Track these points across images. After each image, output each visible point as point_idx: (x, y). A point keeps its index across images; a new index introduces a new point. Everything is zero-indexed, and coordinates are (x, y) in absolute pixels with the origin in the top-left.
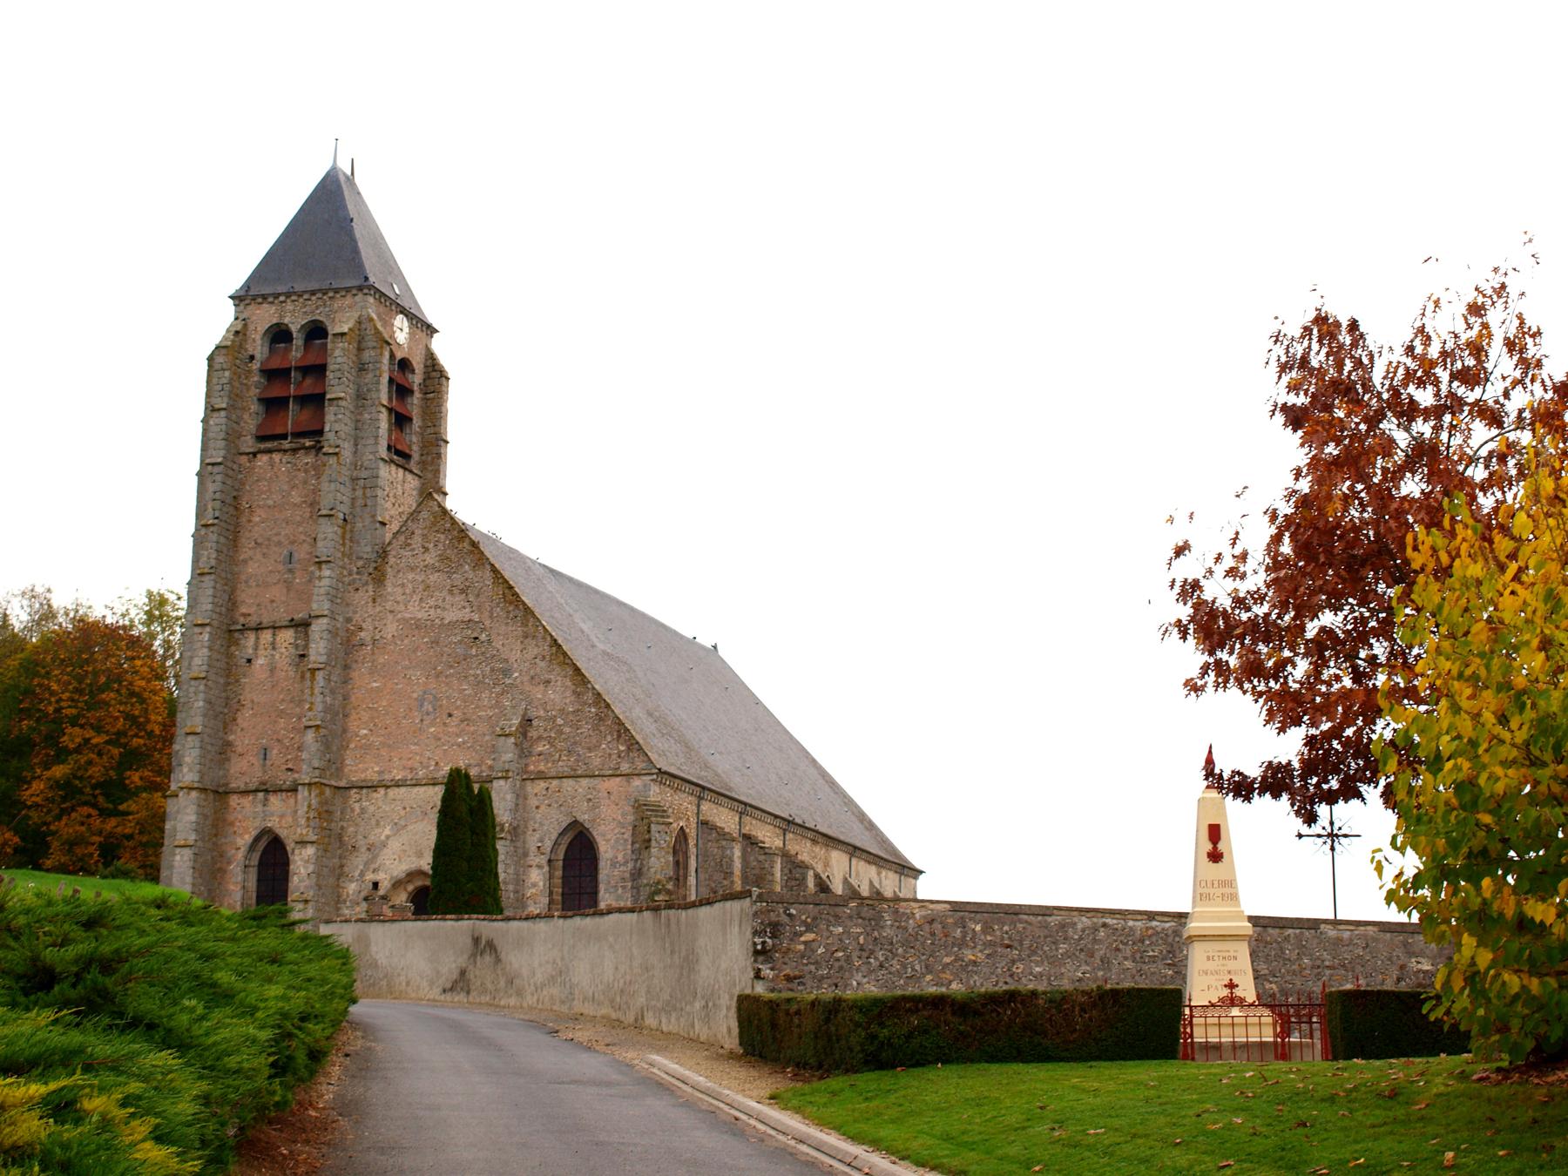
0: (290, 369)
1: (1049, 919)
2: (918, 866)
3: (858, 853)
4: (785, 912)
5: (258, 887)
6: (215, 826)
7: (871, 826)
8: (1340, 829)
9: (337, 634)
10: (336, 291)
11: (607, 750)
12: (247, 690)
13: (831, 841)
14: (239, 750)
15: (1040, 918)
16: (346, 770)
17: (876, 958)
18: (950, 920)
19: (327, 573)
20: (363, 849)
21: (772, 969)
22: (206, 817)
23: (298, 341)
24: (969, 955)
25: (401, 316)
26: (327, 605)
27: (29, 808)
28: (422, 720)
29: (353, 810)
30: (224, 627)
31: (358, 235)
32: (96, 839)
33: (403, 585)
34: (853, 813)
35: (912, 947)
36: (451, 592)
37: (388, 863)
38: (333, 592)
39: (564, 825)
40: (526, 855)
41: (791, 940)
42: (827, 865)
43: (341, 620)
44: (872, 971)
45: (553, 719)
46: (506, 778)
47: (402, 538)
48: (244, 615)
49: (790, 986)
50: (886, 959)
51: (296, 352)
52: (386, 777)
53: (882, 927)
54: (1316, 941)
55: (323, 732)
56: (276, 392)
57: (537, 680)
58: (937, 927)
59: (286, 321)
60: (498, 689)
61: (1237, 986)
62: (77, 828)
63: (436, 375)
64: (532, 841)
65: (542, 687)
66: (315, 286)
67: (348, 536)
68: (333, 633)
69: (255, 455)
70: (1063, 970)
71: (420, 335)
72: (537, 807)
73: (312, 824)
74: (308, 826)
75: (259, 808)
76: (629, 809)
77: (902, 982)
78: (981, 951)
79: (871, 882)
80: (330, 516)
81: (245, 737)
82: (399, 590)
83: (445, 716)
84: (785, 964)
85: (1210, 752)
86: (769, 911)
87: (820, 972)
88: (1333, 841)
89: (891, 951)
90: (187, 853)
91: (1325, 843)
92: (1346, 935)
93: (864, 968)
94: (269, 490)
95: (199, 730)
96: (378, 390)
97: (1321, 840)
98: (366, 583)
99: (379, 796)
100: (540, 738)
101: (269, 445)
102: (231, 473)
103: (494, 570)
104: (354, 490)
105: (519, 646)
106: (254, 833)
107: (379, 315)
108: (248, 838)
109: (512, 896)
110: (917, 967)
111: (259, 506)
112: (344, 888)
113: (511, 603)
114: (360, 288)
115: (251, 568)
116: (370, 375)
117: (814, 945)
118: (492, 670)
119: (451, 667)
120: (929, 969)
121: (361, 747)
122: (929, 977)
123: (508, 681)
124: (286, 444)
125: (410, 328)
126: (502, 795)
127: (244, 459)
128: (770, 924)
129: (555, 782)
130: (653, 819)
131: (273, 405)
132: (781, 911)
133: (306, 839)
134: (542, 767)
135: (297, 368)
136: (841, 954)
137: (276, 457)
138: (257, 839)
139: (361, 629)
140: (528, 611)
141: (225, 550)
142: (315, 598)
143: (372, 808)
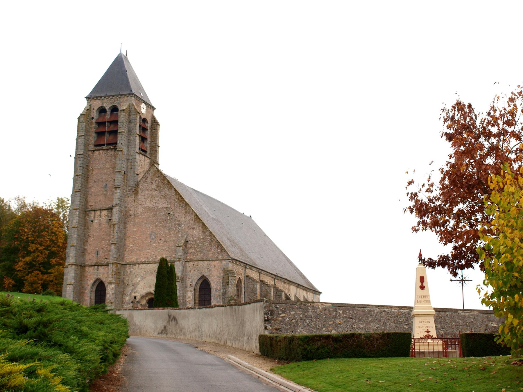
1: (365, 309)
2: (320, 291)
3: (300, 286)
4: (275, 306)
6: (80, 278)
7: (304, 277)
9: (122, 212)
10: (121, 95)
13: (290, 282)
14: (89, 251)
15: (362, 309)
16: (125, 258)
17: (306, 322)
18: (331, 309)
19: (118, 191)
20: (131, 285)
21: (271, 326)
23: (108, 112)
24: (338, 321)
25: (143, 104)
28: (151, 241)
29: (127, 272)
30: (84, 210)
33: (144, 195)
34: (298, 273)
35: (319, 319)
36: (160, 197)
37: (139, 290)
39: (199, 277)
40: (186, 287)
41: (277, 316)
42: (289, 290)
43: (123, 207)
45: (196, 241)
47: (144, 179)
48: (91, 206)
49: (276, 331)
50: (310, 323)
51: (108, 116)
52: (139, 261)
55: (117, 245)
56: (101, 130)
58: (327, 312)
59: (104, 105)
60: (177, 231)
61: (430, 332)
63: (155, 124)
64: (188, 282)
65: (191, 230)
67: (126, 179)
68: (121, 212)
69: (94, 151)
70: (370, 326)
72: (190, 271)
73: (114, 277)
74: (112, 277)
75: (96, 271)
77: (315, 330)
78: (342, 320)
81: (91, 247)
82: (143, 197)
83: (159, 240)
84: (275, 324)
85: (420, 252)
87: (287, 327)
88: (463, 282)
89: (311, 320)
90: (71, 286)
92: (467, 314)
93: (302, 326)
95: (75, 245)
96: (136, 129)
98: (132, 195)
99: (136, 267)
100: (191, 247)
101: (99, 148)
103: (175, 190)
104: (128, 163)
106: (94, 280)
107: (136, 104)
108: (92, 282)
109: (181, 301)
110: (320, 325)
111: (95, 169)
114: (129, 94)
115: (93, 190)
117: (285, 318)
118: (175, 224)
121: (130, 251)
122: (324, 329)
123: (180, 228)
124: (104, 147)
125: (146, 108)
126: (178, 267)
127: (90, 153)
128: (270, 311)
129: (196, 262)
130: (230, 275)
131: (100, 134)
132: (274, 306)
133: (111, 282)
134: (192, 257)
135: (108, 122)
137: (101, 152)
138: (95, 282)
139: (130, 210)
140: (187, 204)
143: (134, 271)
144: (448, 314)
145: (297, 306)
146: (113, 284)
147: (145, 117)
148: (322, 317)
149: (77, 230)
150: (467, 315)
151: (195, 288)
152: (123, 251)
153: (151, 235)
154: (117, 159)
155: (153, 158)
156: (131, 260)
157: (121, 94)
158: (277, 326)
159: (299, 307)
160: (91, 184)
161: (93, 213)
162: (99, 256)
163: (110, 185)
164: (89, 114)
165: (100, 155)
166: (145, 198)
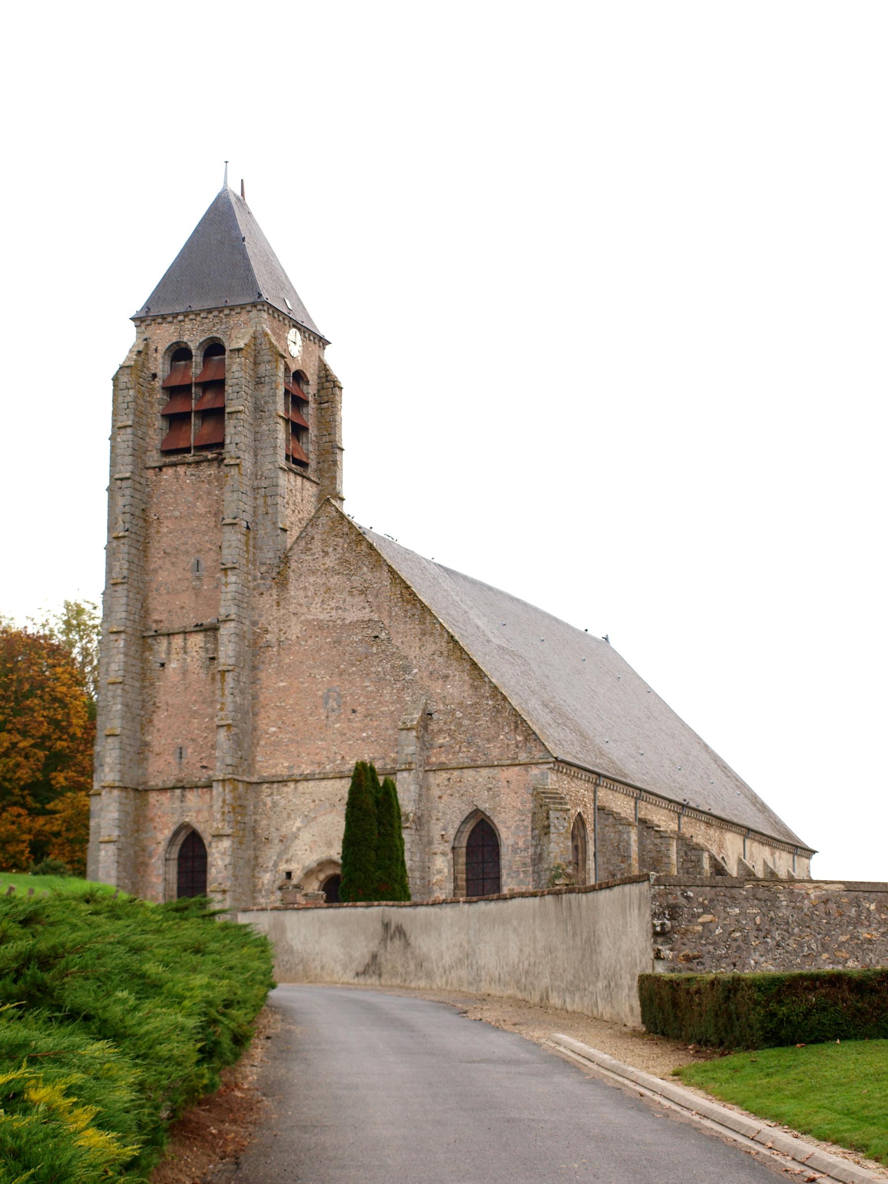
2: (812, 846)
3: (751, 835)
7: (763, 809)
9: (244, 637)
10: (231, 309)
12: (162, 692)
13: (725, 824)
14: (157, 750)
16: (257, 766)
17: (773, 938)
18: (845, 900)
19: (232, 578)
20: (276, 841)
21: (671, 950)
22: (127, 814)
23: (197, 358)
24: (864, 934)
25: (294, 330)
28: (327, 717)
29: (265, 804)
30: (138, 634)
31: (250, 253)
32: (26, 837)
33: (305, 588)
35: (808, 927)
36: (351, 593)
37: (299, 853)
38: (239, 597)
39: (466, 813)
40: (430, 843)
41: (689, 921)
42: (721, 846)
43: (248, 623)
46: (409, 770)
47: (303, 543)
49: (689, 965)
50: (783, 938)
51: (196, 369)
52: (296, 771)
55: (234, 730)
56: (179, 407)
57: (436, 675)
58: (832, 906)
59: (185, 339)
64: (436, 830)
65: (440, 682)
66: (212, 305)
67: (251, 543)
68: (241, 636)
69: (160, 468)
72: (440, 797)
73: (227, 818)
74: (224, 820)
75: (177, 804)
77: (799, 960)
78: (876, 930)
79: (765, 863)
82: (301, 593)
83: (349, 712)
84: (684, 944)
86: (667, 894)
90: (112, 848)
93: (761, 948)
94: (175, 502)
95: (118, 732)
96: (275, 402)
98: (270, 588)
99: (289, 790)
100: (440, 731)
101: (173, 459)
102: (138, 486)
103: (391, 571)
104: (256, 499)
105: (417, 644)
106: (173, 828)
107: (273, 330)
108: (168, 833)
109: (418, 882)
110: (814, 946)
112: (259, 878)
113: (408, 602)
114: (254, 305)
115: (161, 577)
116: (267, 388)
117: (712, 926)
118: (393, 667)
119: (353, 665)
120: (825, 948)
121: (271, 744)
122: (825, 956)
123: (408, 677)
124: (189, 458)
125: (303, 341)
126: (406, 786)
127: (150, 473)
128: (668, 907)
129: (456, 773)
130: (552, 806)
132: (679, 893)
133: (222, 832)
134: (443, 759)
135: (197, 384)
136: (738, 934)
137: (181, 470)
138: (176, 834)
139: (267, 632)
140: (425, 609)
141: (136, 560)
142: (222, 603)
143: (283, 802)
146: (225, 839)
147: (301, 368)
149: (123, 689)
151: (456, 845)
152: (250, 747)
153: (326, 699)
156: (273, 771)
158: (690, 949)
160: (155, 562)
161: (164, 641)
162: (184, 761)
163: (208, 561)
164: (143, 365)
165: (177, 477)
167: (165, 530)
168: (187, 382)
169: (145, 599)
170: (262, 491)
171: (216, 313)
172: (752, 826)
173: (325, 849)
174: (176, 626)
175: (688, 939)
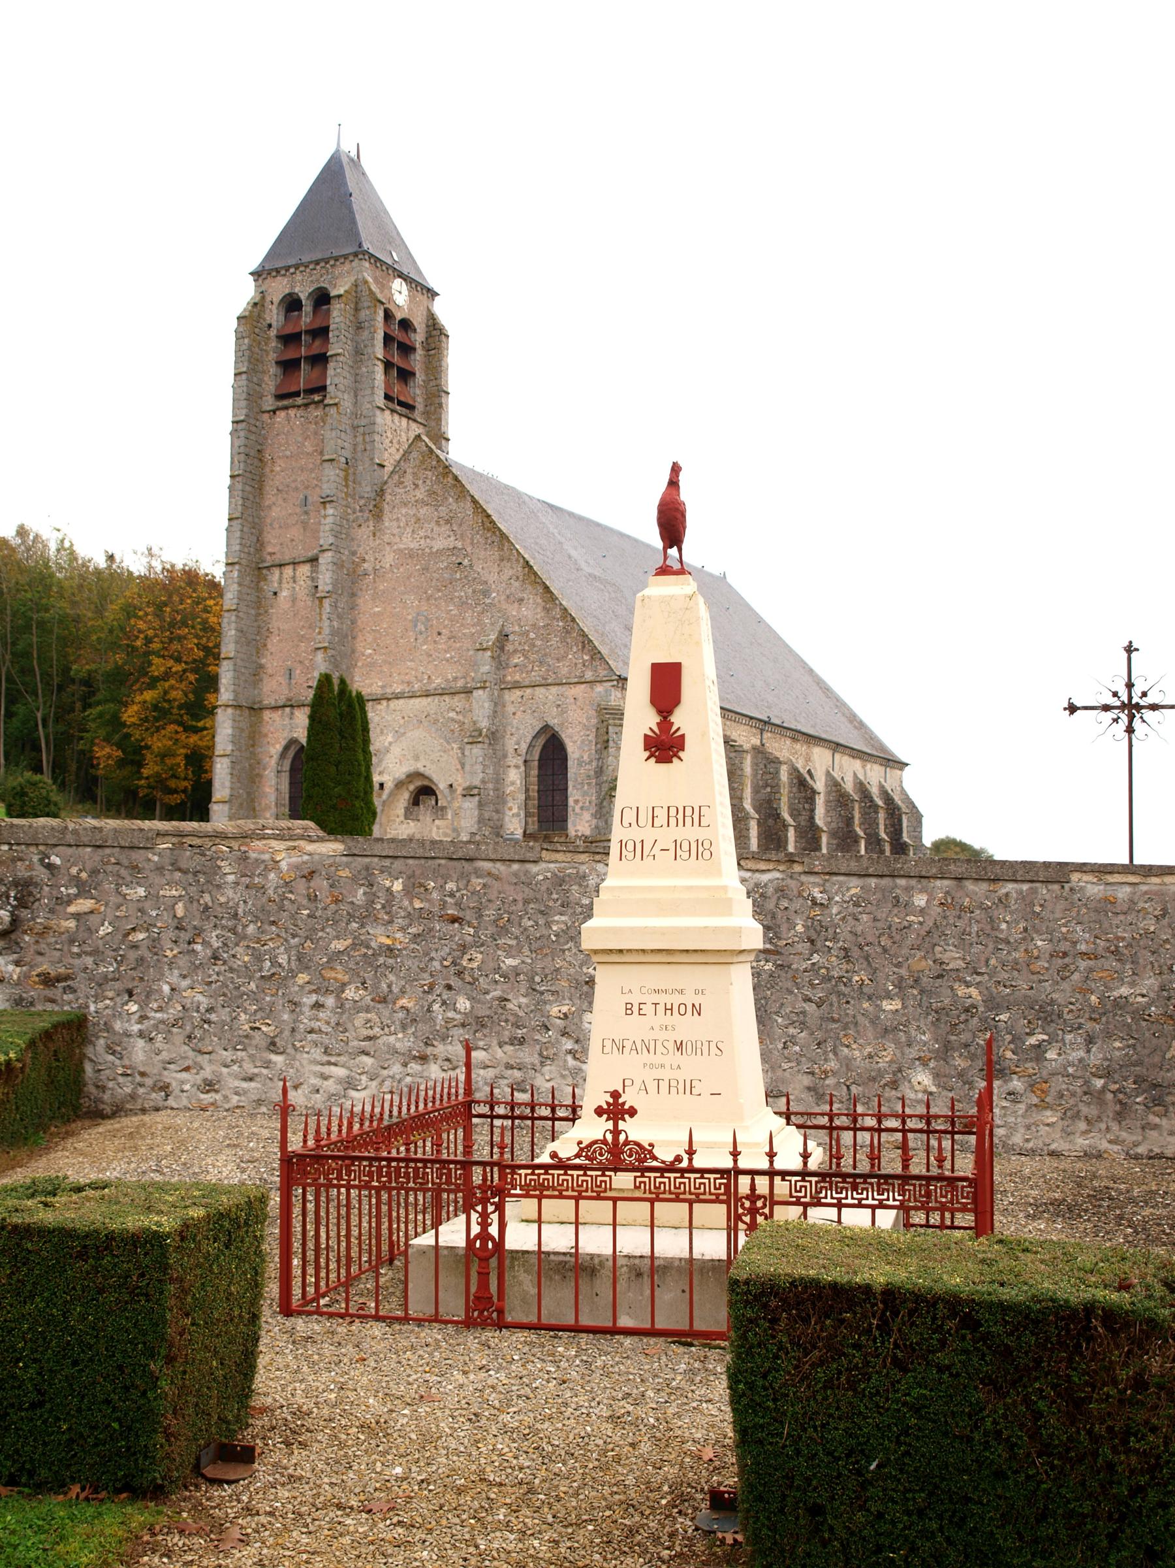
0: (300, 333)
1: (534, 868)
2: (904, 760)
3: (841, 749)
4: (41, 860)
5: (291, 788)
6: (250, 738)
7: (860, 726)
8: (1144, 694)
9: (343, 566)
10: (336, 259)
11: (571, 661)
12: (274, 618)
13: (813, 739)
14: (270, 671)
15: (516, 866)
17: (206, 944)
18: (345, 873)
19: (330, 511)
21: (17, 963)
22: (242, 730)
23: (308, 307)
24: (379, 936)
25: (399, 280)
26: (331, 540)
27: (129, 726)
30: (254, 565)
31: (355, 207)
32: (183, 751)
33: (398, 519)
34: (843, 714)
35: (273, 923)
36: (438, 523)
39: (537, 729)
40: (505, 756)
41: (52, 911)
42: (808, 759)
43: (346, 553)
44: (197, 967)
45: (527, 633)
46: (484, 688)
47: (396, 477)
48: (271, 554)
49: (49, 993)
50: (225, 944)
51: (306, 318)
52: (389, 690)
53: (219, 887)
54: (1062, 905)
55: (331, 652)
56: (291, 354)
57: (512, 599)
58: (321, 884)
59: (296, 290)
60: (479, 609)
61: (632, 1112)
62: (165, 742)
63: (436, 332)
64: (510, 744)
65: (516, 604)
66: (320, 256)
67: (351, 478)
68: (338, 565)
69: (274, 412)
70: (559, 963)
71: (420, 297)
72: (514, 714)
75: (287, 721)
76: (593, 713)
77: (253, 986)
78: (402, 929)
79: (855, 774)
80: (332, 460)
81: (272, 662)
82: (395, 524)
83: (435, 634)
84: (41, 954)
85: (673, 484)
86: (14, 860)
87: (102, 969)
88: (1131, 718)
89: (233, 930)
90: (226, 761)
91: (1116, 720)
92: (1123, 893)
93: (183, 961)
94: (287, 443)
95: (231, 655)
96: (373, 346)
97: (1110, 715)
98: (368, 520)
100: (515, 651)
101: (285, 402)
102: (254, 429)
103: (474, 501)
104: (355, 436)
105: (496, 569)
106: (284, 743)
107: (376, 279)
108: (279, 748)
109: (491, 793)
110: (283, 959)
111: (279, 457)
113: (488, 530)
114: (356, 255)
115: (275, 513)
116: (366, 333)
117: (93, 920)
118: (474, 592)
119: (439, 590)
120: (303, 962)
122: (302, 978)
123: (488, 601)
124: (299, 401)
125: (409, 291)
127: (266, 417)
128: (16, 884)
129: (529, 691)
130: (611, 722)
131: (289, 366)
132: (35, 859)
134: (517, 678)
135: (306, 332)
136: (141, 936)
137: (292, 412)
138: (286, 748)
139: (364, 560)
140: (503, 536)
141: (251, 497)
142: (321, 534)
144: (1007, 895)
145: (156, 858)
148: (293, 917)
149: (237, 616)
150: (1120, 895)
152: (348, 668)
153: (415, 623)
154: (328, 427)
155: (433, 424)
157: (335, 254)
158: (52, 963)
159: (167, 861)
160: (270, 497)
161: (277, 571)
162: (293, 682)
163: (314, 498)
164: (259, 316)
165: (288, 420)
166: (399, 527)
167: (278, 469)
168: (297, 330)
169: (261, 532)
170: (361, 430)
171: (322, 264)
172: (842, 742)
173: (412, 762)
174: (287, 558)
175: (48, 944)
